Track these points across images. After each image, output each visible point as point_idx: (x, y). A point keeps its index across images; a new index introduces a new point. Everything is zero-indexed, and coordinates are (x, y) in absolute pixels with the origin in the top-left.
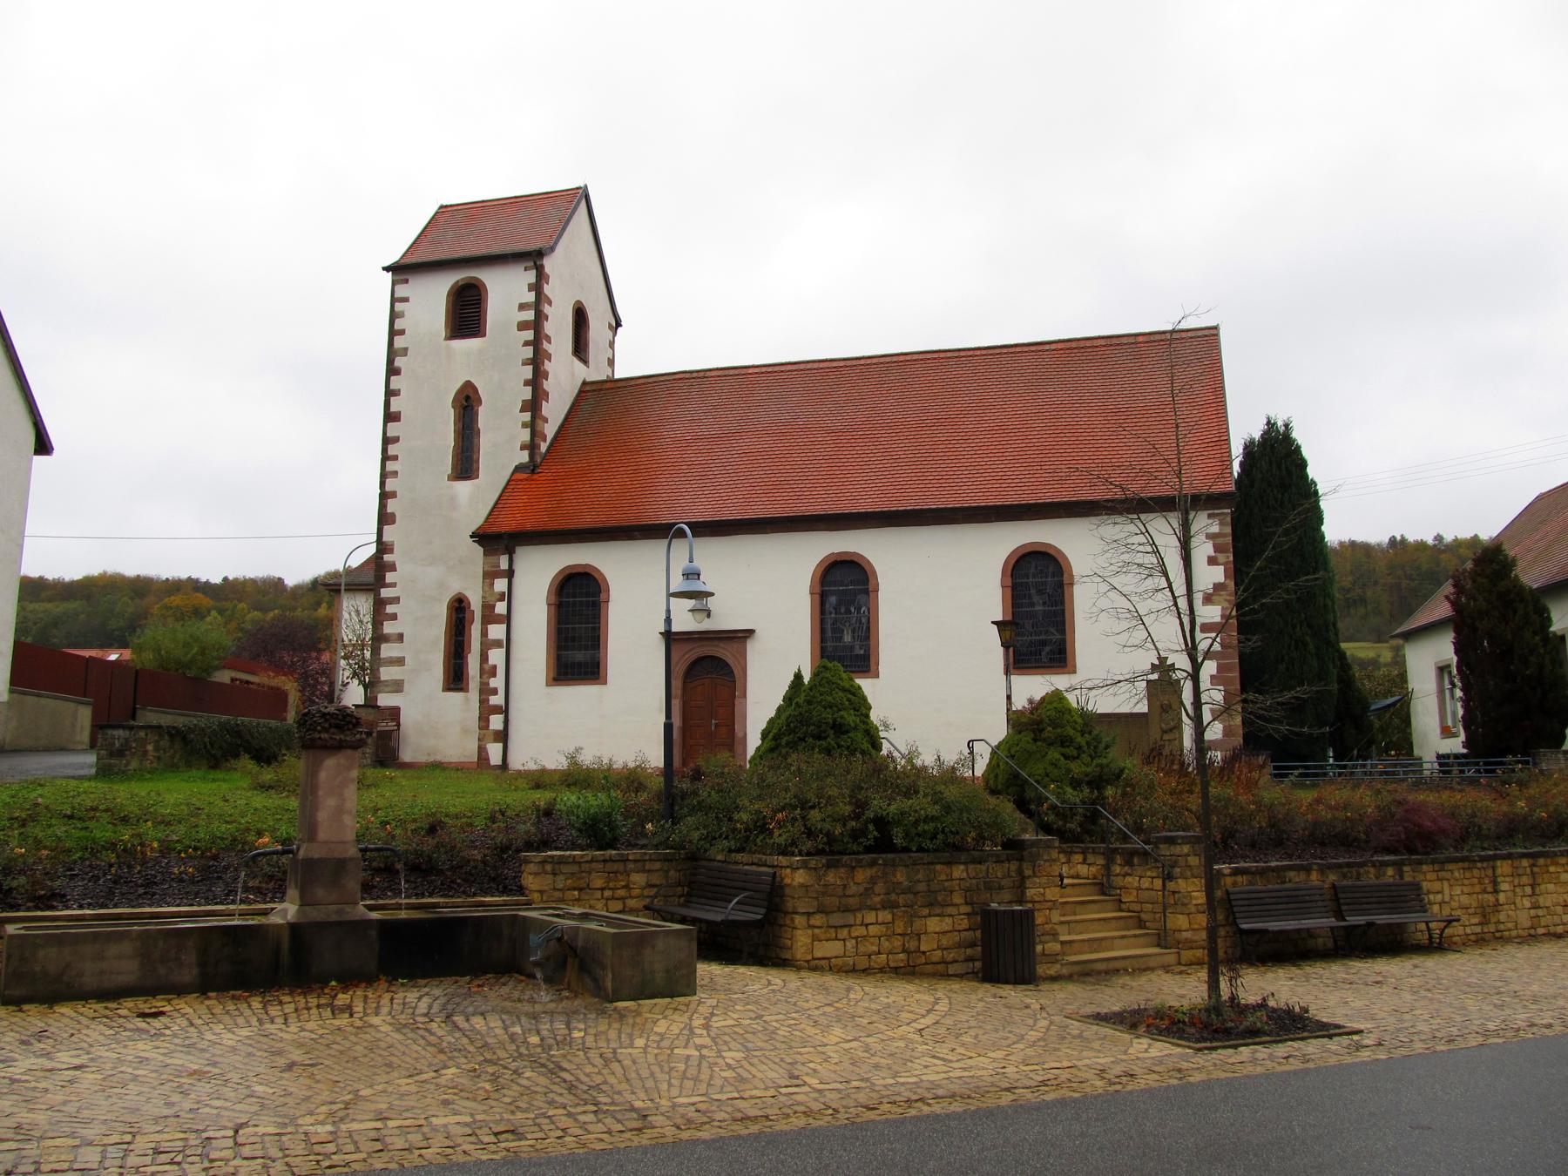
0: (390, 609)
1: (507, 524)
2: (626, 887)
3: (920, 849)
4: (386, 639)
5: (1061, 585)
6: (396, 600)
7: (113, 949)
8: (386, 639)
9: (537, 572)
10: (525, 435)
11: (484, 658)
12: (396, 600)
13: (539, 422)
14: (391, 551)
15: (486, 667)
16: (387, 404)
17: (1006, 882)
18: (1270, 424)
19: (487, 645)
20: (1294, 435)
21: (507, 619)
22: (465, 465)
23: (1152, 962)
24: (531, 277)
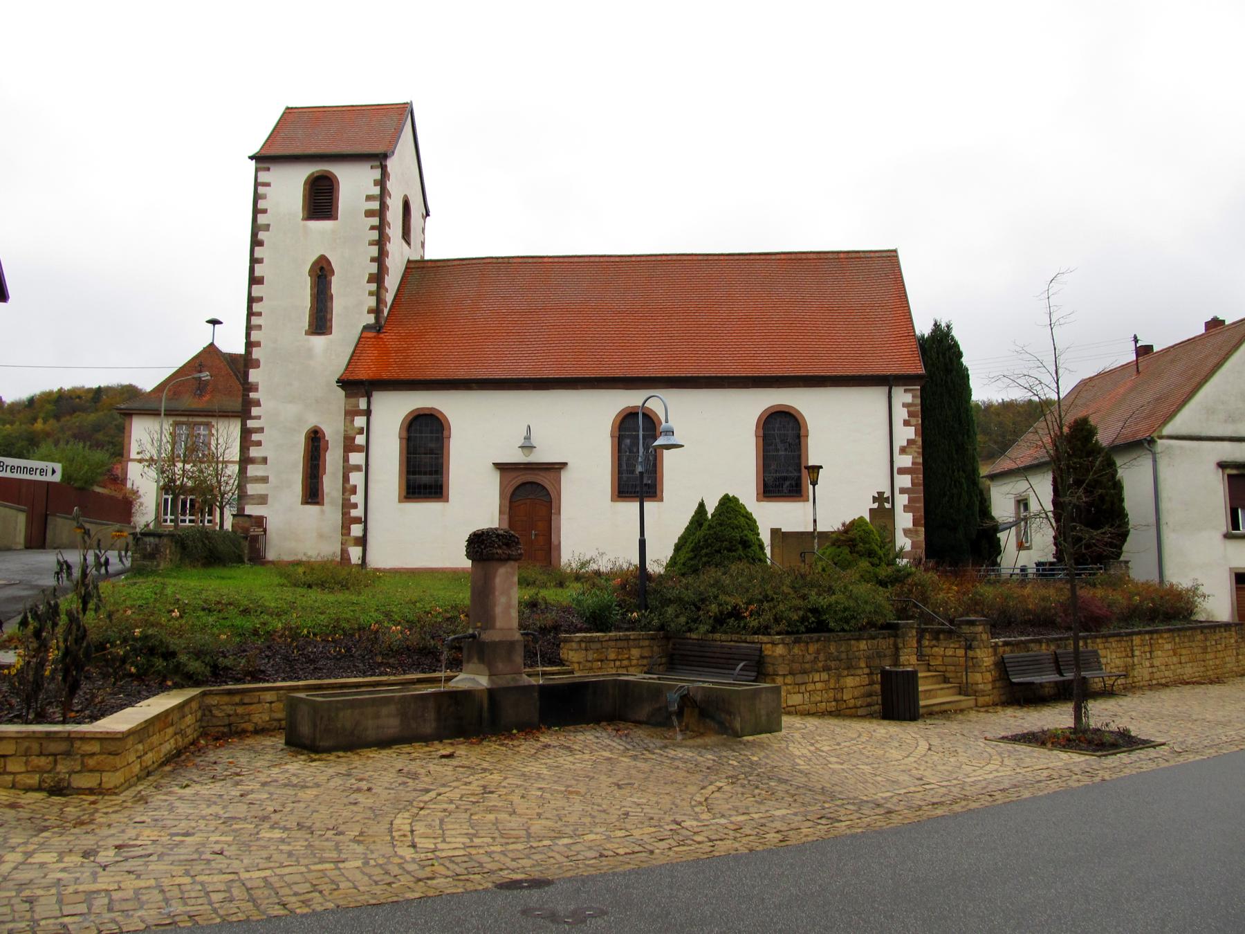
0: (255, 437)
1: (363, 374)
2: (629, 659)
3: (843, 630)
4: (252, 461)
5: (799, 437)
6: (261, 430)
7: (384, 711)
8: (252, 461)
9: (390, 413)
10: (372, 302)
11: (346, 479)
12: (261, 430)
13: (383, 291)
14: (256, 390)
15: (348, 486)
16: (252, 270)
17: (888, 652)
18: (937, 326)
19: (347, 469)
20: (954, 333)
21: (366, 449)
22: (320, 322)
23: (963, 705)
24: (377, 174)
